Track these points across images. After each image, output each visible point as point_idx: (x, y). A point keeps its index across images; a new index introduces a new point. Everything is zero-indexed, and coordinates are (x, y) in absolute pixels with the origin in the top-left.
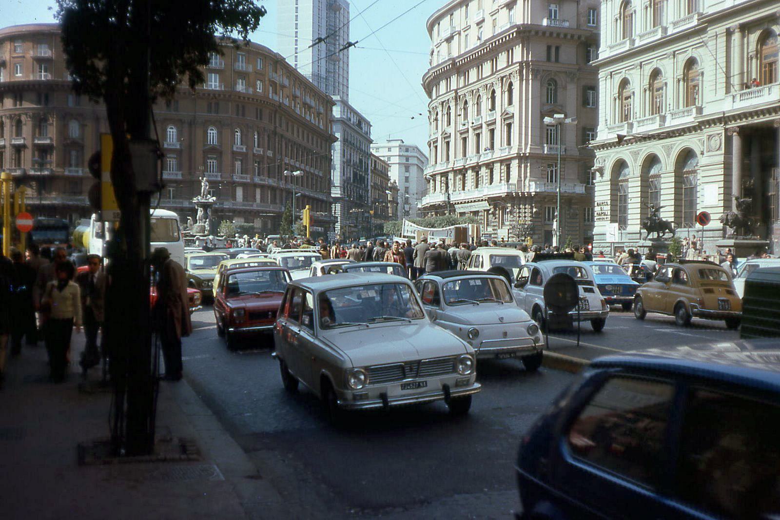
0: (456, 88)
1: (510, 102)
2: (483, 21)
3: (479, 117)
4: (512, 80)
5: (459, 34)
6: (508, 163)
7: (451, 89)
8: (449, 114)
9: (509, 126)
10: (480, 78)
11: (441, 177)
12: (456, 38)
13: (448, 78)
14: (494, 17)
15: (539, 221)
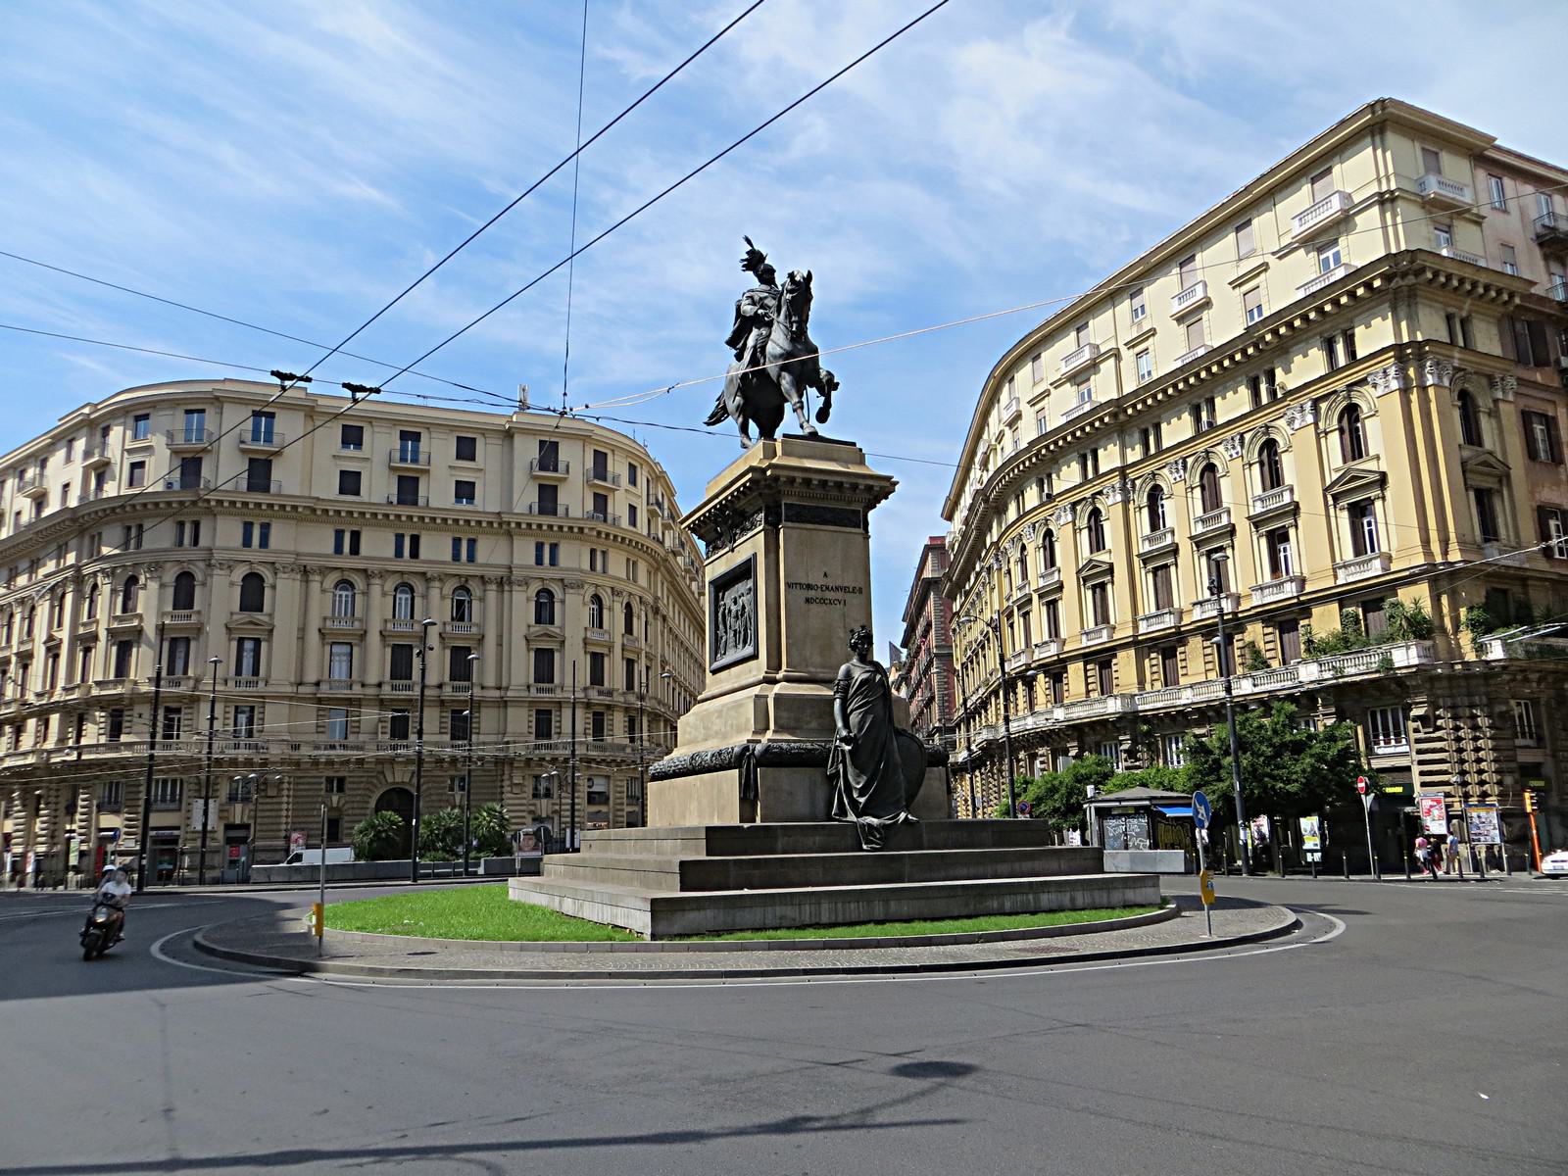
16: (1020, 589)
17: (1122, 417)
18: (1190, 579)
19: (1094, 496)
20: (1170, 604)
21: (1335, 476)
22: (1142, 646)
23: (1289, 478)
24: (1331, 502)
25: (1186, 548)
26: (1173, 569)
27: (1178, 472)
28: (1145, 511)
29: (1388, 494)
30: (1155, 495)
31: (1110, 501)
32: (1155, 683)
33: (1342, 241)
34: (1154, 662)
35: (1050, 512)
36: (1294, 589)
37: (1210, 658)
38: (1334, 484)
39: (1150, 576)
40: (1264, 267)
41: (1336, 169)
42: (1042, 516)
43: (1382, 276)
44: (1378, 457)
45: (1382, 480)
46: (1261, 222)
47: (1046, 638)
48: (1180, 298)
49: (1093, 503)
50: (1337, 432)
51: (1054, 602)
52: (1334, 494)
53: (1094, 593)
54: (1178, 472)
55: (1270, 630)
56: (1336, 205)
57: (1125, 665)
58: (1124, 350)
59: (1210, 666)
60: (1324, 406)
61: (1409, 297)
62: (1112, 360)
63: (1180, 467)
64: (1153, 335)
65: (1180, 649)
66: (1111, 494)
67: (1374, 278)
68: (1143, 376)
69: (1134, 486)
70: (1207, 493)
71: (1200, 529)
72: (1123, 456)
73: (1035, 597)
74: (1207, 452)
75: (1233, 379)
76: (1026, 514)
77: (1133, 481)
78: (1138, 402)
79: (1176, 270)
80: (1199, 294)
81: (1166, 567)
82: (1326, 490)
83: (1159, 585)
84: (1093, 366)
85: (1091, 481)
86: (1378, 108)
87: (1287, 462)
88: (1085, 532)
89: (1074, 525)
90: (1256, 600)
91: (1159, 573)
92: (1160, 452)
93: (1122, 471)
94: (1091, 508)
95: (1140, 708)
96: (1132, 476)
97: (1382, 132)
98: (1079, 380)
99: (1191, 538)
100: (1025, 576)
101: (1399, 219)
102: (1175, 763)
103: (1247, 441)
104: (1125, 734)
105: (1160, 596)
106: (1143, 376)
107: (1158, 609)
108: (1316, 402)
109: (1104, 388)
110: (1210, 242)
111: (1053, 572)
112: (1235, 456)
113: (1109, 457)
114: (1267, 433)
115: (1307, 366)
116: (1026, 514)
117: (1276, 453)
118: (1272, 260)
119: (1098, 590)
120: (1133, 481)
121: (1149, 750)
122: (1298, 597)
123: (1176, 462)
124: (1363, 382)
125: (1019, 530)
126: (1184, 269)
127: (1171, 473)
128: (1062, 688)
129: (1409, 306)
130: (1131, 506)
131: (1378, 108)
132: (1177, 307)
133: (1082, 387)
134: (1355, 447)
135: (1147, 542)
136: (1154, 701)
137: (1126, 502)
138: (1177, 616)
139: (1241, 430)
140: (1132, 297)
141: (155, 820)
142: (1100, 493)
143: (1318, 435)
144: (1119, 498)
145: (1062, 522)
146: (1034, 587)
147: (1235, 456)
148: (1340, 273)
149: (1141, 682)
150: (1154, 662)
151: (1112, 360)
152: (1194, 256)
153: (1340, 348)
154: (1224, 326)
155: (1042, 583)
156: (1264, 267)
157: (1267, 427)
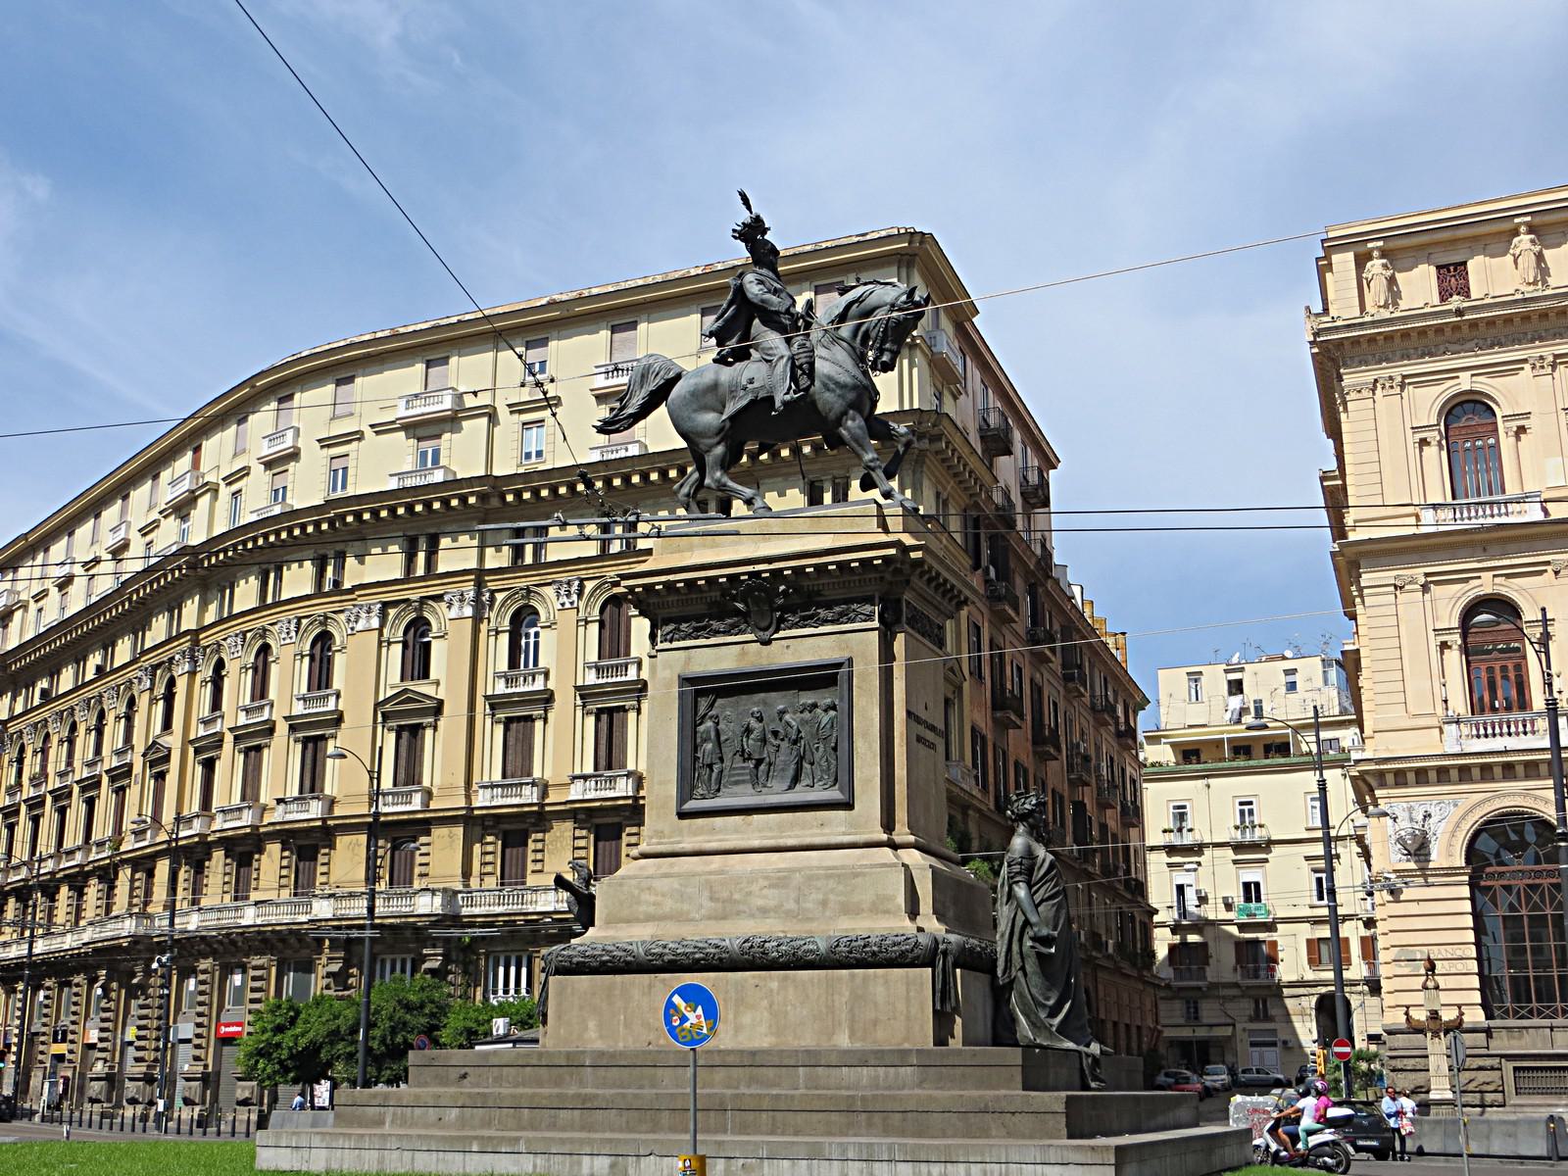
0: (194, 627)
1: (167, 725)
2: (294, 455)
3: (218, 713)
4: (223, 655)
5: (214, 491)
6: (149, 866)
7: (183, 629)
8: (169, 698)
9: (160, 777)
10: (269, 600)
11: (134, 872)
12: (204, 502)
13: (174, 607)
14: (148, 538)
15: (1492, 1069)
16: (206, 722)
17: (495, 502)
18: (282, 763)
19: (423, 600)
20: (257, 799)
21: (390, 693)
22: (476, 824)
23: (337, 683)
24: (380, 719)
25: (565, 701)
26: (539, 724)
27: (568, 595)
28: (505, 639)
29: (645, 705)
30: (523, 618)
31: (454, 613)
32: (487, 879)
33: (446, 436)
34: (490, 848)
35: (336, 607)
36: (535, 795)
37: (489, 858)
38: (387, 701)
39: (499, 729)
40: (359, 436)
41: (642, 327)
42: (258, 624)
43: (477, 494)
44: (437, 683)
45: (438, 709)
46: (365, 385)
47: (236, 800)
48: (271, 438)
49: (420, 609)
50: (400, 645)
51: (258, 749)
52: (384, 712)
53: (398, 738)
54: (568, 595)
55: (584, 833)
56: (447, 403)
57: (442, 852)
58: (503, 413)
59: (284, 881)
60: (392, 612)
61: (916, 462)
62: (485, 420)
63: (292, 627)
64: (359, 439)
65: (256, 856)
66: (456, 604)
67: (366, 510)
68: (528, 456)
69: (492, 600)
70: (607, 633)
71: (591, 678)
72: (481, 558)
73: (229, 738)
74: (528, 590)
75: (786, 476)
76: (232, 617)
77: (493, 592)
78: (526, 489)
79: (605, 334)
80: (288, 441)
81: (530, 719)
82: (377, 705)
83: (511, 742)
84: (451, 421)
85: (269, 607)
86: (917, 238)
87: (339, 661)
88: (397, 649)
89: (381, 634)
90: (576, 792)
91: (514, 726)
92: (537, 565)
93: (480, 575)
94: (413, 615)
95: (465, 911)
96: (492, 586)
97: (910, 265)
98: (421, 432)
99: (577, 688)
100: (216, 704)
101: (915, 371)
102: (501, 993)
103: (587, 591)
104: (434, 946)
105: (510, 758)
106: (528, 456)
107: (504, 776)
108: (386, 605)
109: (463, 456)
110: (673, 312)
111: (262, 708)
112: (568, 605)
113: (457, 554)
114: (324, 623)
115: (384, 564)
116: (232, 617)
117: (329, 649)
118: (369, 433)
119: (405, 735)
120: (493, 592)
121: (465, 972)
122: (324, 820)
123: (569, 583)
124: (438, 598)
125: (219, 637)
126: (283, 406)
127: (559, 595)
128: (249, 875)
129: (914, 472)
130: (484, 627)
131: (917, 238)
132: (266, 450)
133: (424, 444)
134: (418, 662)
135: (502, 681)
136: (486, 903)
137: (477, 619)
138: (327, 804)
139: (583, 574)
140: (339, 383)
141: (1437, 1049)
142: (438, 598)
143: (380, 643)
144: (468, 611)
145: (360, 626)
146: (229, 723)
147: (568, 605)
148: (438, 477)
149: (466, 874)
150: (490, 848)
151: (485, 420)
152: (448, 358)
153: (421, 556)
154: (307, 488)
155: (242, 720)
156: (359, 436)
157: (265, 630)
